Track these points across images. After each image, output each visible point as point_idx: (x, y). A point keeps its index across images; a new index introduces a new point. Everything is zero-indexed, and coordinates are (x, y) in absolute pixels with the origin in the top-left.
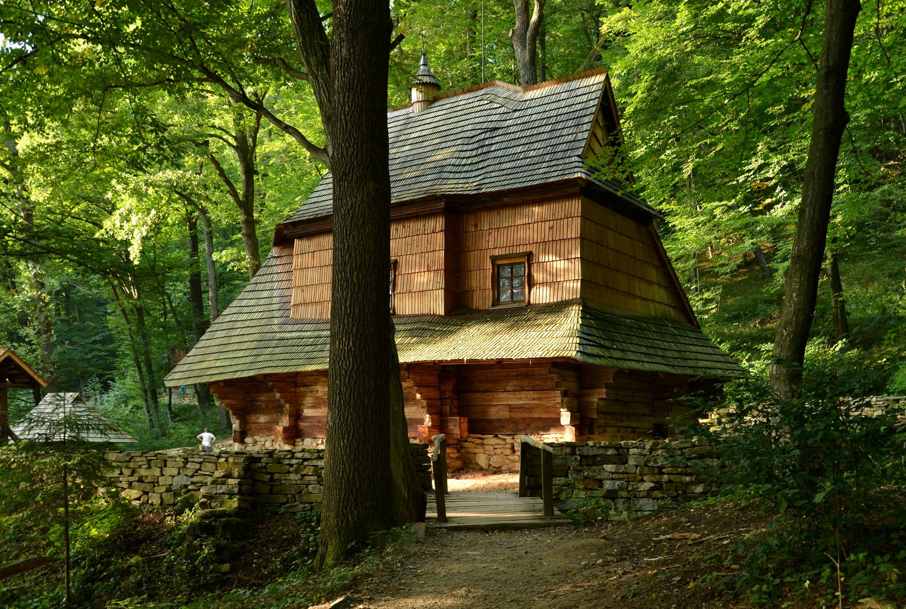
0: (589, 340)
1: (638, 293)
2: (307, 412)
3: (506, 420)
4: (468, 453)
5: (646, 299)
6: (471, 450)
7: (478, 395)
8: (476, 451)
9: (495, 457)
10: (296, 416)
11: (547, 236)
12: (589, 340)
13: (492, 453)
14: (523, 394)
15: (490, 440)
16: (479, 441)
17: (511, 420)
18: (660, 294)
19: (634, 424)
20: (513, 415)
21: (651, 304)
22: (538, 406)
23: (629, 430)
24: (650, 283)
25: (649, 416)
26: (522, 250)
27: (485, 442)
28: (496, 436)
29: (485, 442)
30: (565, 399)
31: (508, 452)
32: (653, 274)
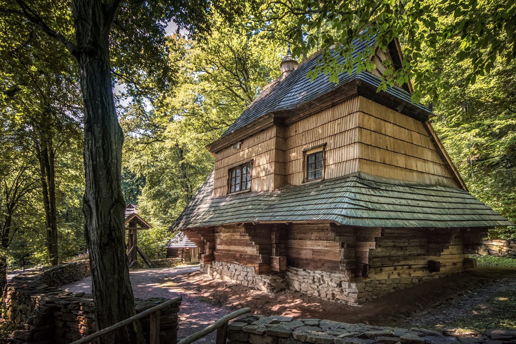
0: (355, 205)
1: (414, 168)
2: (218, 247)
3: (310, 260)
4: (290, 279)
5: (422, 172)
6: (291, 277)
7: (295, 241)
8: (294, 278)
9: (304, 284)
10: (213, 248)
11: (336, 130)
12: (355, 205)
13: (302, 281)
14: (321, 242)
15: (301, 272)
16: (295, 272)
17: (313, 260)
18: (437, 169)
19: (410, 263)
20: (314, 256)
21: (426, 176)
22: (329, 251)
23: (405, 267)
24: (425, 161)
25: (424, 255)
26: (321, 142)
27: (298, 273)
28: (305, 270)
29: (298, 273)
30: (343, 249)
31: (311, 281)
32: (429, 155)
